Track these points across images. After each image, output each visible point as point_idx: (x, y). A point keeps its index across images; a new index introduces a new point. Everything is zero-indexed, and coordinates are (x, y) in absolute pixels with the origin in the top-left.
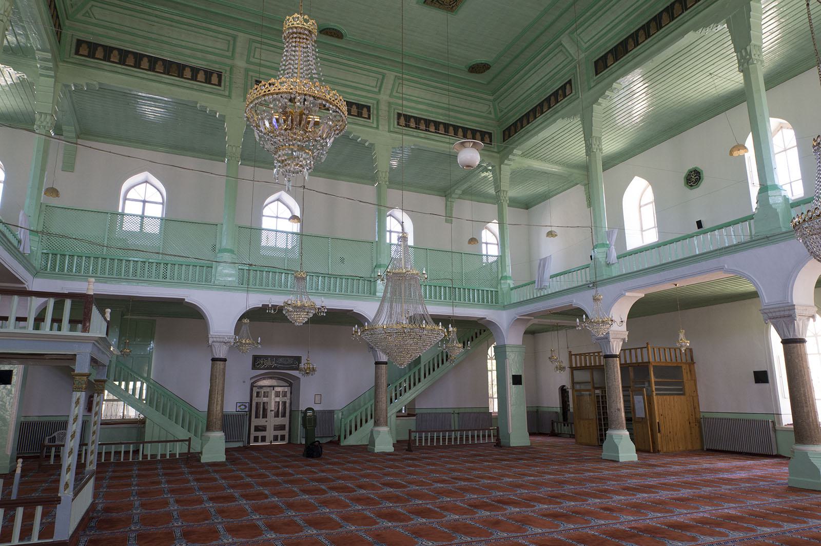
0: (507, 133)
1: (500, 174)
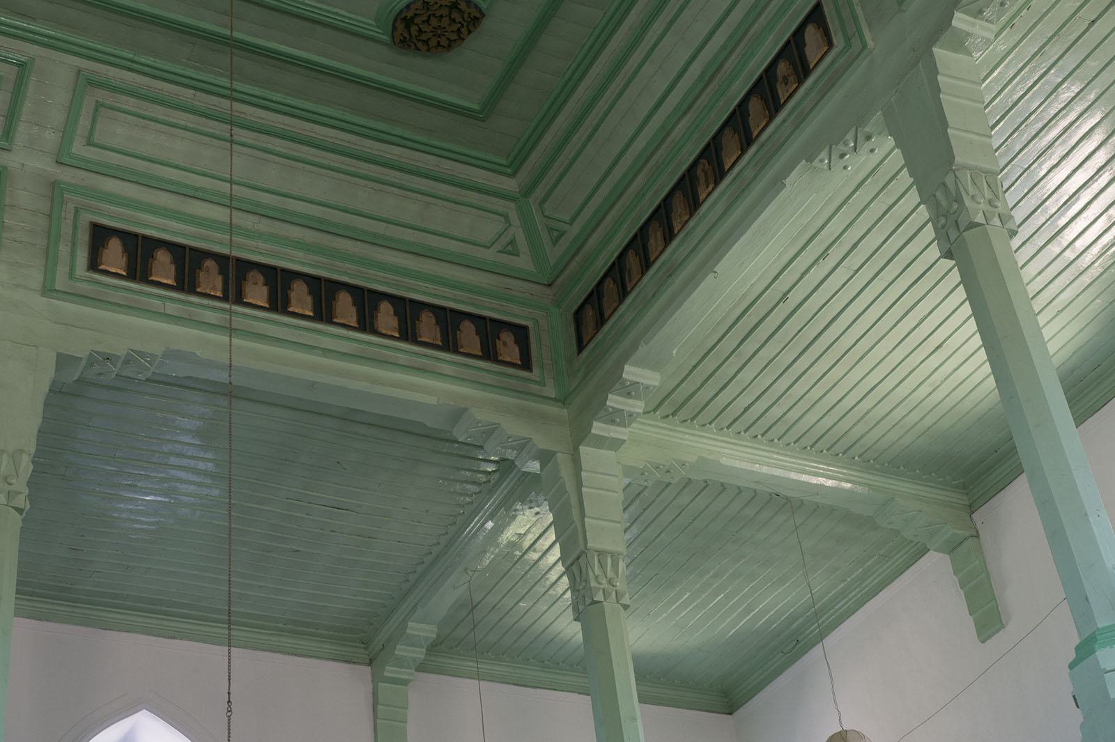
0: (589, 313)
1: (579, 484)
